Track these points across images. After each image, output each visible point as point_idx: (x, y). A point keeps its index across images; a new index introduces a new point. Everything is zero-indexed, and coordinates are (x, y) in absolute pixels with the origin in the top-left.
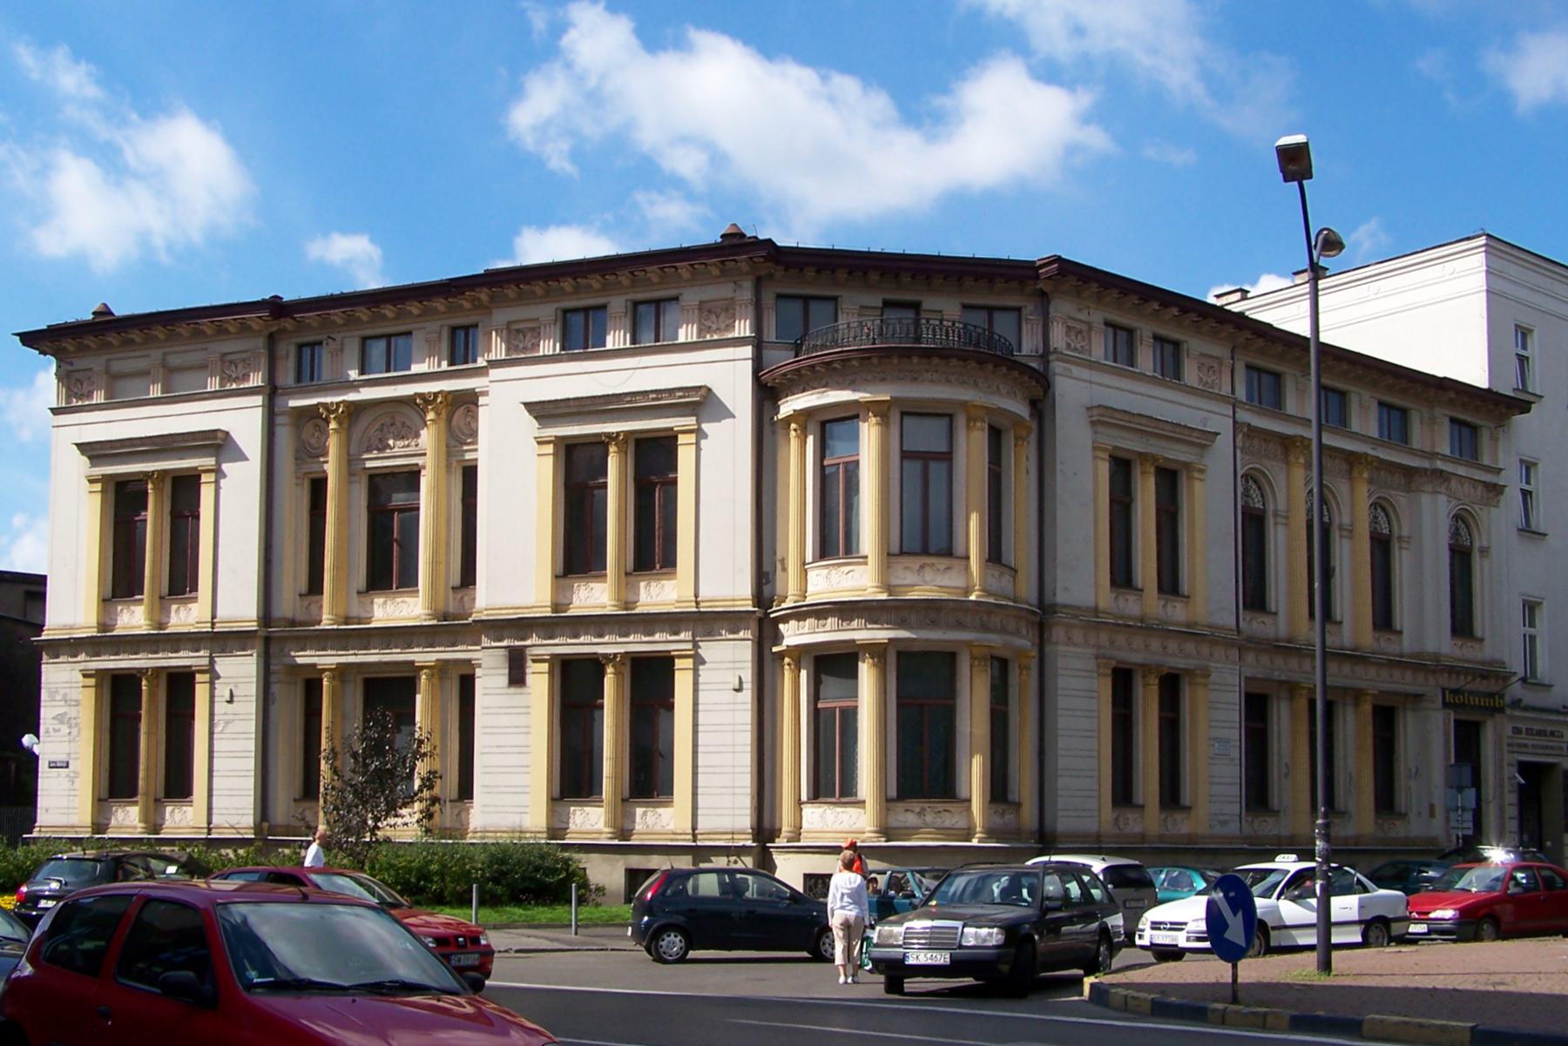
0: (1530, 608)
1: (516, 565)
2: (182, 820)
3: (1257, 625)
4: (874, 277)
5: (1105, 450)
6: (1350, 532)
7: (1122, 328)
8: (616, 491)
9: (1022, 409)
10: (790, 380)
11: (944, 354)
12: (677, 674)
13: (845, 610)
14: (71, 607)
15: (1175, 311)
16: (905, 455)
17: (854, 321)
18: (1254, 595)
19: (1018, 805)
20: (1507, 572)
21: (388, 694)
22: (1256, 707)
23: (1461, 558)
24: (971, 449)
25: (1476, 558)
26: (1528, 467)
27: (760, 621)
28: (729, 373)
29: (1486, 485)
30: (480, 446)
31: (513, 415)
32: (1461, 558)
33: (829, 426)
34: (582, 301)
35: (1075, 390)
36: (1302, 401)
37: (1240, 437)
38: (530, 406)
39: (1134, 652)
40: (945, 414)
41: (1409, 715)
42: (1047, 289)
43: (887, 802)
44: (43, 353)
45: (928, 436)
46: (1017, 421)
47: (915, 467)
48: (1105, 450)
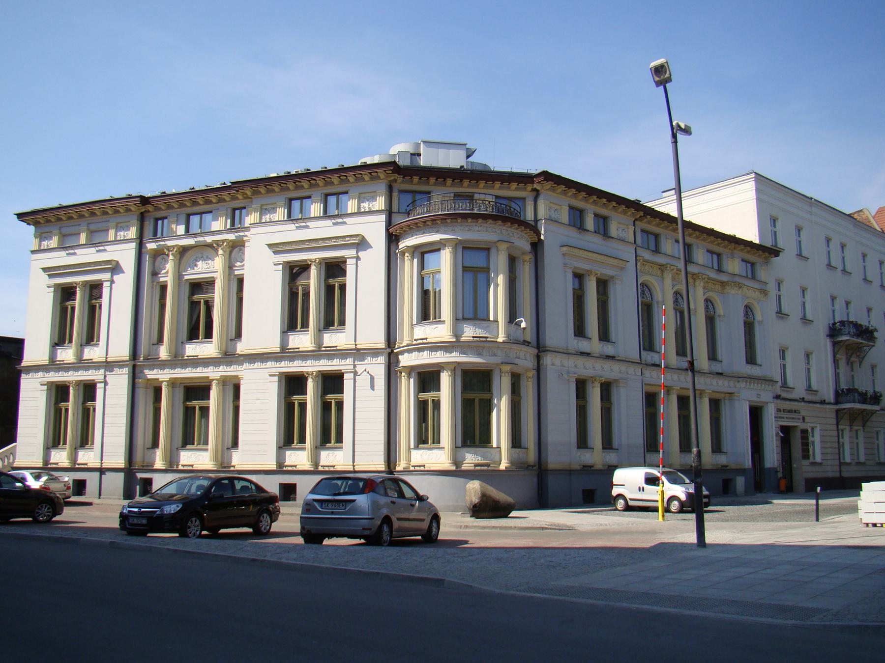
2: (335, 459)
3: (649, 357)
4: (449, 181)
8: (315, 292)
10: (405, 231)
11: (485, 217)
13: (435, 347)
14: (35, 352)
15: (604, 200)
16: (465, 269)
17: (440, 200)
18: (648, 342)
20: (771, 335)
21: (197, 391)
22: (651, 399)
23: (749, 328)
24: (500, 260)
27: (390, 354)
28: (374, 229)
30: (245, 267)
31: (264, 248)
32: (749, 328)
33: (422, 252)
34: (293, 188)
36: (670, 247)
38: (270, 246)
42: (538, 188)
43: (456, 448)
44: (28, 224)
45: (477, 260)
47: (469, 276)
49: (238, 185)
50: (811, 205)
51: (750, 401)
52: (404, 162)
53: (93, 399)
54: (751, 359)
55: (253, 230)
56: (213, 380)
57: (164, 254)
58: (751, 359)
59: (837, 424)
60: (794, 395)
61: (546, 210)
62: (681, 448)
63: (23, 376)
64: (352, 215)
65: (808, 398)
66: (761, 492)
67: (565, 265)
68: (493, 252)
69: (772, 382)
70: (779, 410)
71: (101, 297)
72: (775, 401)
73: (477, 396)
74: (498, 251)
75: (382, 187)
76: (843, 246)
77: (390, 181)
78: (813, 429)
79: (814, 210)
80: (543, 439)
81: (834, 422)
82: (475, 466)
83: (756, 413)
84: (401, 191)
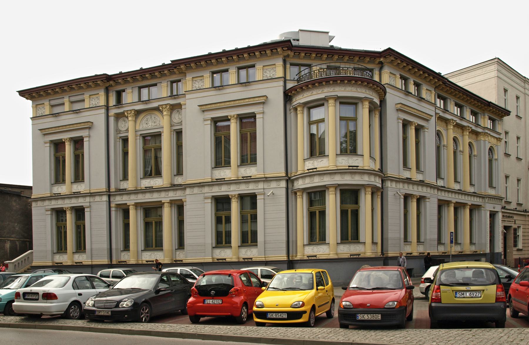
0: (507, 177)
5: (401, 119)
8: (233, 138)
16: (341, 119)
20: (504, 166)
29: (497, 138)
33: (310, 106)
35: (393, 99)
40: (353, 102)
41: (477, 211)
44: (27, 99)
45: (348, 111)
47: (344, 123)
48: (401, 119)
49: (176, 64)
51: (490, 211)
53: (84, 219)
56: (164, 203)
61: (387, 77)
67: (398, 118)
68: (360, 105)
69: (501, 199)
74: (363, 108)
75: (279, 63)
77: (285, 57)
80: (384, 237)
82: (351, 255)
84: (292, 64)
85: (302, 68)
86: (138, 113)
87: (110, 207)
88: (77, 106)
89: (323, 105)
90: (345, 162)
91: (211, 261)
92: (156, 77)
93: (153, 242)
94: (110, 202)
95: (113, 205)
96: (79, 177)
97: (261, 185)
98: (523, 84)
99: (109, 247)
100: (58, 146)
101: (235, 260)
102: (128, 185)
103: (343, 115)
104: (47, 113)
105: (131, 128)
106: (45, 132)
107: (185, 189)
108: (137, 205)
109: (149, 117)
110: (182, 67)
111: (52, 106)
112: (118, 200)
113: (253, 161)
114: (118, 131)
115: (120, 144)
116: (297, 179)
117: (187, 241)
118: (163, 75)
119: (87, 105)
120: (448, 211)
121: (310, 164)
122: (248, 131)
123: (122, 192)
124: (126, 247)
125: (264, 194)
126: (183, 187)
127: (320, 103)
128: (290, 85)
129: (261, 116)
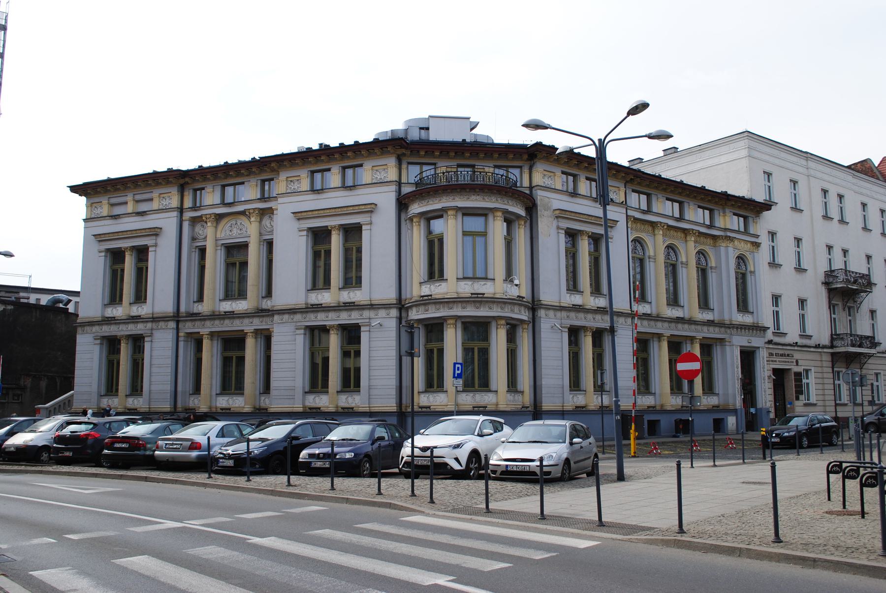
1: (291, 281)
6: (686, 264)
7: (571, 174)
9: (522, 213)
12: (362, 334)
16: (465, 234)
19: (522, 392)
20: (765, 283)
22: (643, 344)
24: (498, 228)
25: (748, 276)
26: (773, 235)
29: (753, 243)
33: (428, 217)
37: (630, 223)
39: (579, 320)
40: (483, 213)
44: (81, 195)
45: (475, 224)
46: (519, 217)
47: (469, 239)
50: (807, 159)
52: (414, 135)
54: (743, 305)
55: (280, 200)
57: (203, 221)
58: (743, 305)
59: (833, 368)
60: (788, 340)
62: (672, 389)
63: (79, 330)
64: (584, 197)
65: (801, 341)
66: (753, 430)
67: (558, 228)
68: (490, 217)
69: (765, 329)
70: (771, 354)
71: (147, 260)
72: (767, 346)
73: (234, 354)
76: (841, 197)
78: (807, 371)
79: (811, 164)
81: (830, 364)
83: (748, 357)
85: (425, 168)
86: (219, 217)
87: (178, 336)
88: (143, 207)
89: (441, 216)
90: (466, 288)
91: (301, 410)
92: (242, 175)
93: (231, 381)
94: (178, 329)
95: (181, 334)
96: (140, 297)
97: (366, 313)
98: (804, 162)
99: (173, 389)
100: (117, 256)
101: (332, 409)
102: (204, 308)
103: (467, 229)
104: (105, 213)
105: (213, 237)
106: (100, 238)
107: (273, 315)
108: (212, 335)
109: (234, 222)
110: (273, 165)
111: (113, 205)
112: (188, 327)
113: (359, 282)
114: (194, 239)
115: (196, 256)
116: (411, 307)
117: (273, 384)
118: (250, 173)
119: (155, 205)
120: (660, 347)
121: (426, 290)
122: (352, 245)
123: (194, 316)
124: (197, 390)
125: (369, 325)
126: (269, 313)
127: (439, 214)
128: (406, 190)
129: (368, 227)
